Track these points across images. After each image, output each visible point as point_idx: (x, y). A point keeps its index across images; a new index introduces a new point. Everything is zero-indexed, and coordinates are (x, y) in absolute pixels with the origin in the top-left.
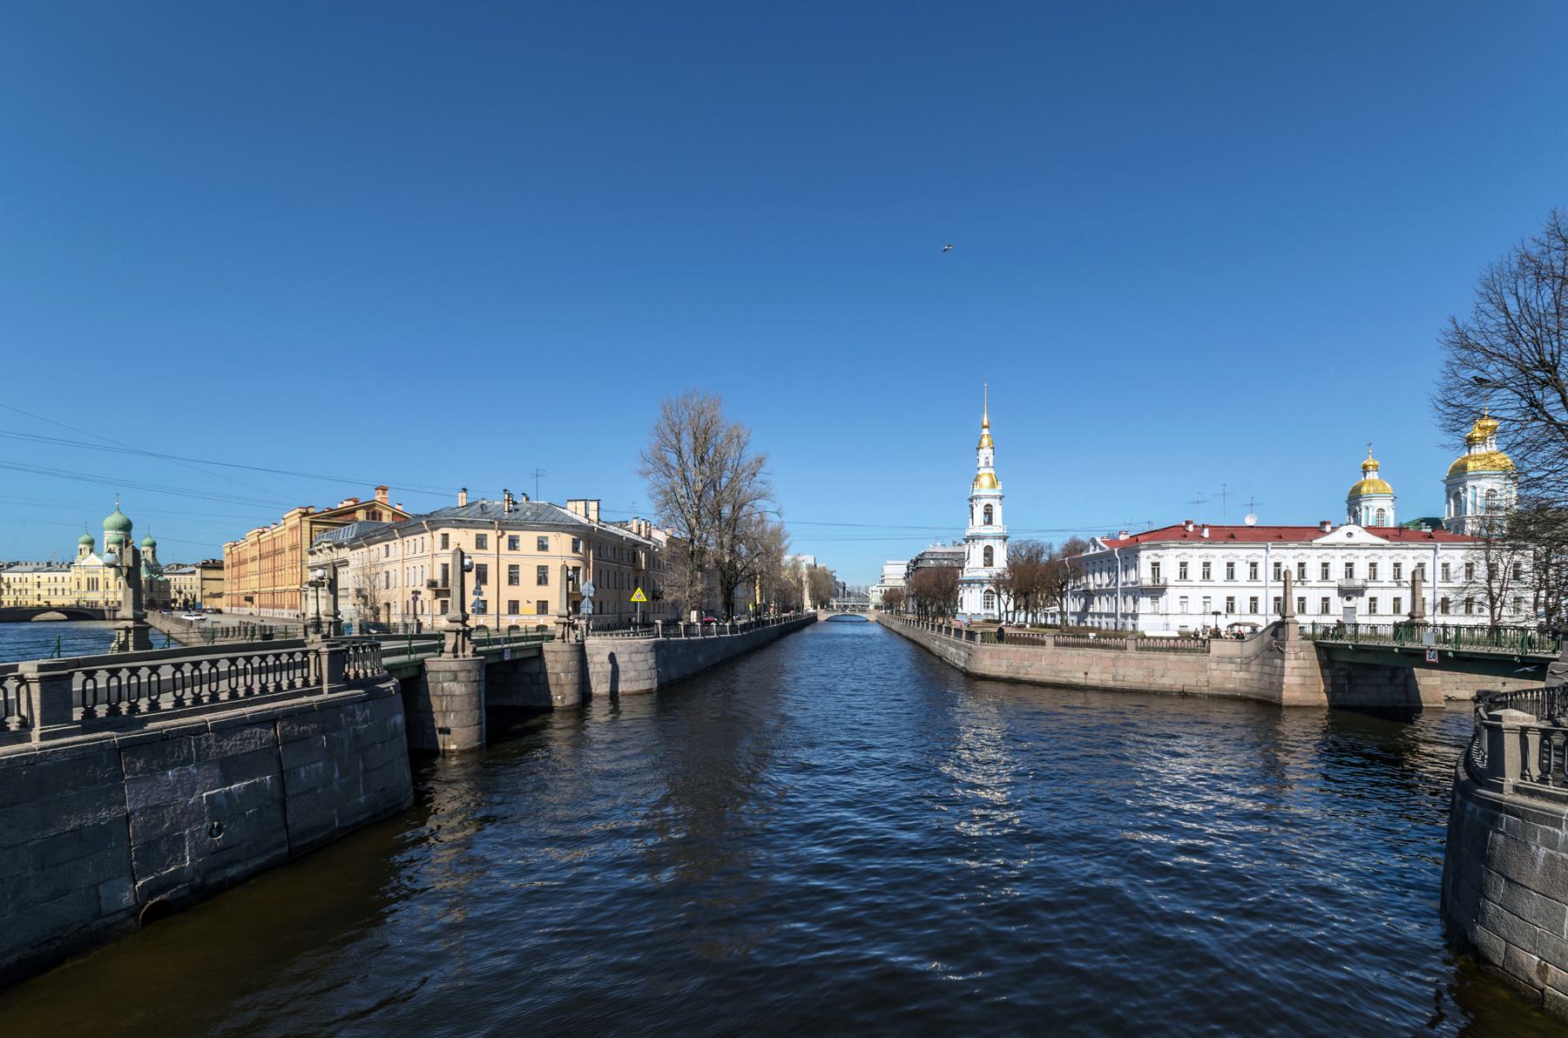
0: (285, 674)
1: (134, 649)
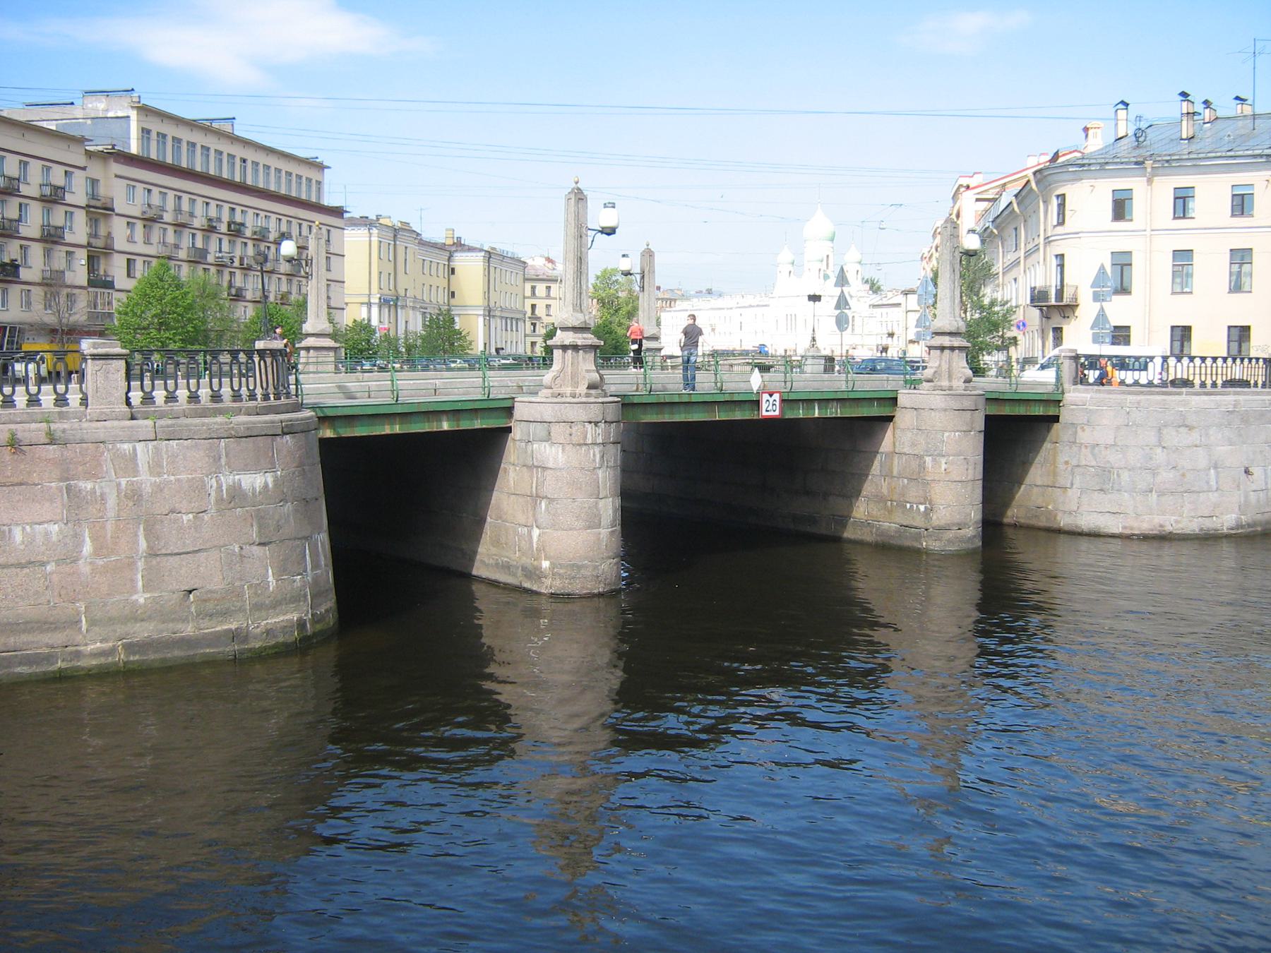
0: (226, 381)
1: (1056, 301)
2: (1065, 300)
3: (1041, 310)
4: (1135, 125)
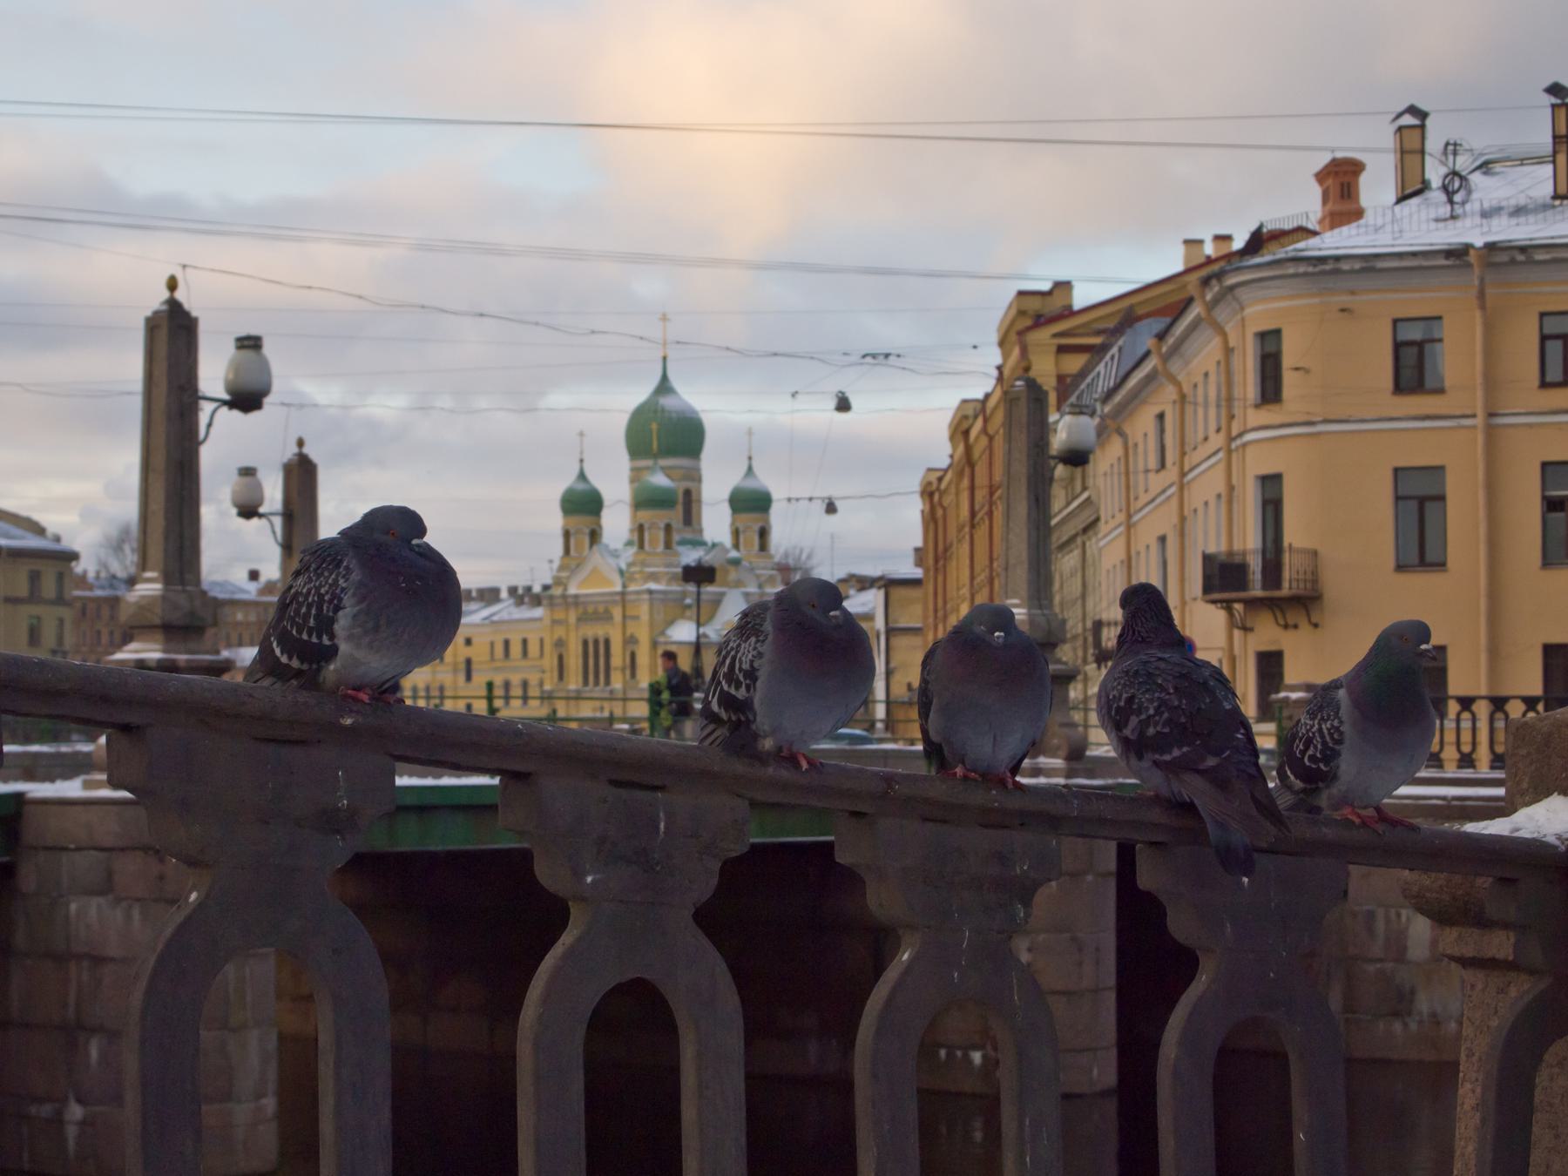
1: (1264, 587)
2: (1286, 584)
3: (1229, 610)
4: (1444, 164)
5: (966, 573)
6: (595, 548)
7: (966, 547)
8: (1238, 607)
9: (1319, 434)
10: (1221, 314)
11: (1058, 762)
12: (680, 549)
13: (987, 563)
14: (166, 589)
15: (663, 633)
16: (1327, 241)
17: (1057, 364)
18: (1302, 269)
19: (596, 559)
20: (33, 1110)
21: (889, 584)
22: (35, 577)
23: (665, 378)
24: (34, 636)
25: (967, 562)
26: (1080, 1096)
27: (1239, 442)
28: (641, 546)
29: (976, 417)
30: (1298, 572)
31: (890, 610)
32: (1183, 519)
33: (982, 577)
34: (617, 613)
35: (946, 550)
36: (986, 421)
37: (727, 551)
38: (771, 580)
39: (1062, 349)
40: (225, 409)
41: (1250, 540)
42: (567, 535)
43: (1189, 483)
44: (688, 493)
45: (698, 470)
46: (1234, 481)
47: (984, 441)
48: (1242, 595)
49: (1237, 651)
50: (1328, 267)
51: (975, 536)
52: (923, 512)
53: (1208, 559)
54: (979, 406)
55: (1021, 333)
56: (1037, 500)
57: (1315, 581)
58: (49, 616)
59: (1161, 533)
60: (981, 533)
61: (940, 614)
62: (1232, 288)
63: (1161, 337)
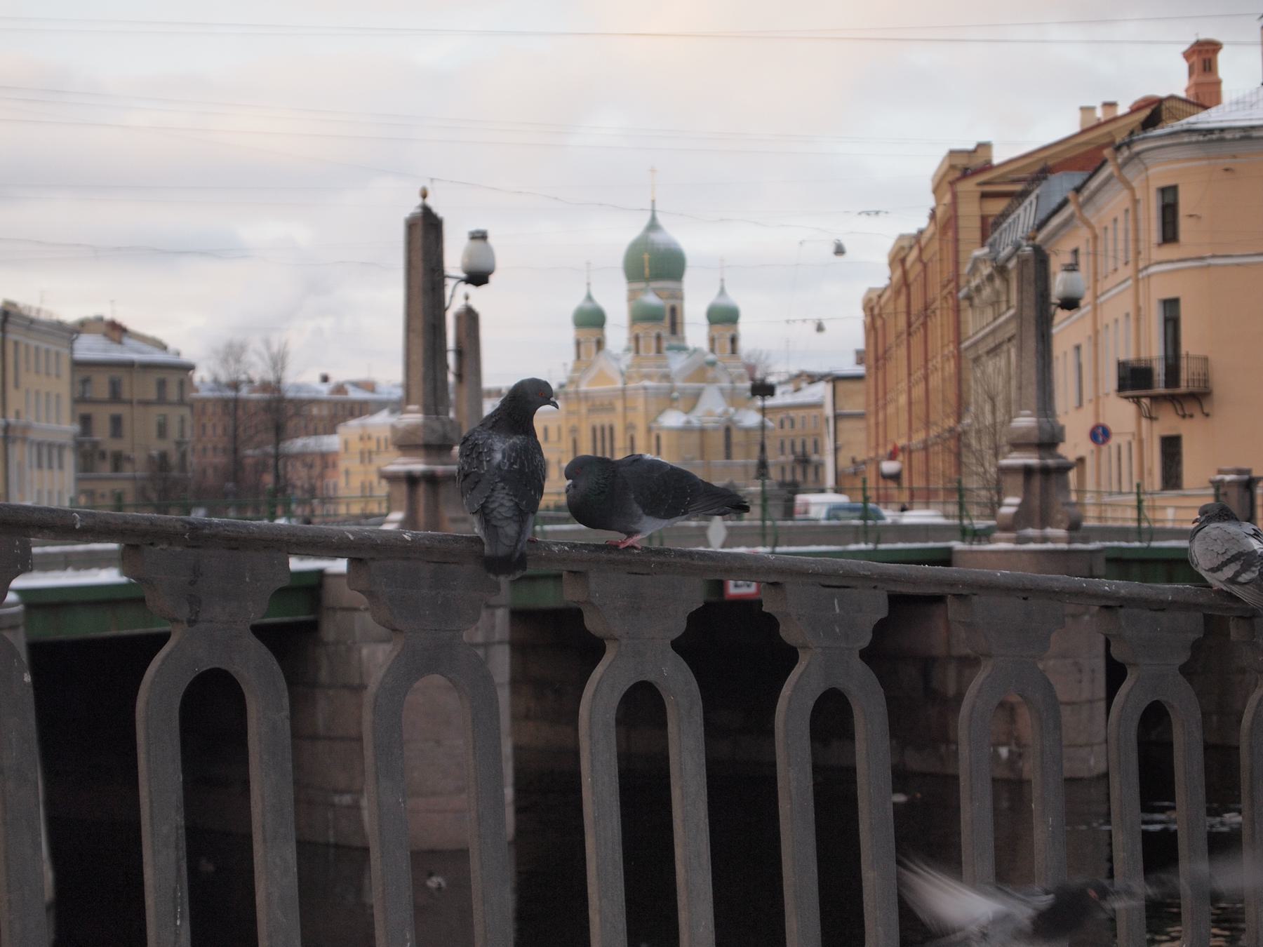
1: (1167, 385)
2: (1183, 384)
5: (904, 371)
6: (601, 353)
7: (903, 351)
8: (1145, 401)
9: (1209, 266)
10: (1129, 173)
11: (1061, 532)
12: (669, 354)
13: (923, 363)
14: (426, 419)
15: (655, 420)
16: (1213, 115)
17: (981, 208)
18: (1194, 138)
19: (602, 362)
20: (336, 799)
21: (836, 380)
22: (162, 384)
23: (653, 219)
24: (162, 431)
25: (905, 363)
26: (1081, 779)
27: (1145, 273)
28: (637, 351)
29: (911, 248)
30: (1199, 375)
31: (837, 398)
32: (1096, 332)
33: (919, 374)
34: (619, 405)
35: (885, 352)
36: (921, 250)
37: (704, 355)
38: (740, 377)
39: (985, 196)
40: (463, 284)
41: (1154, 351)
42: (578, 344)
43: (1101, 304)
44: (673, 310)
45: (681, 290)
46: (1141, 303)
47: (919, 267)
48: (1150, 392)
49: (1144, 435)
50: (1214, 137)
51: (912, 342)
52: (865, 323)
53: (1122, 365)
54: (913, 241)
55: (952, 183)
56: (1043, 336)
57: (1206, 381)
58: (174, 415)
59: (1076, 342)
60: (917, 339)
61: (881, 402)
62: (1138, 154)
63: (1078, 190)
